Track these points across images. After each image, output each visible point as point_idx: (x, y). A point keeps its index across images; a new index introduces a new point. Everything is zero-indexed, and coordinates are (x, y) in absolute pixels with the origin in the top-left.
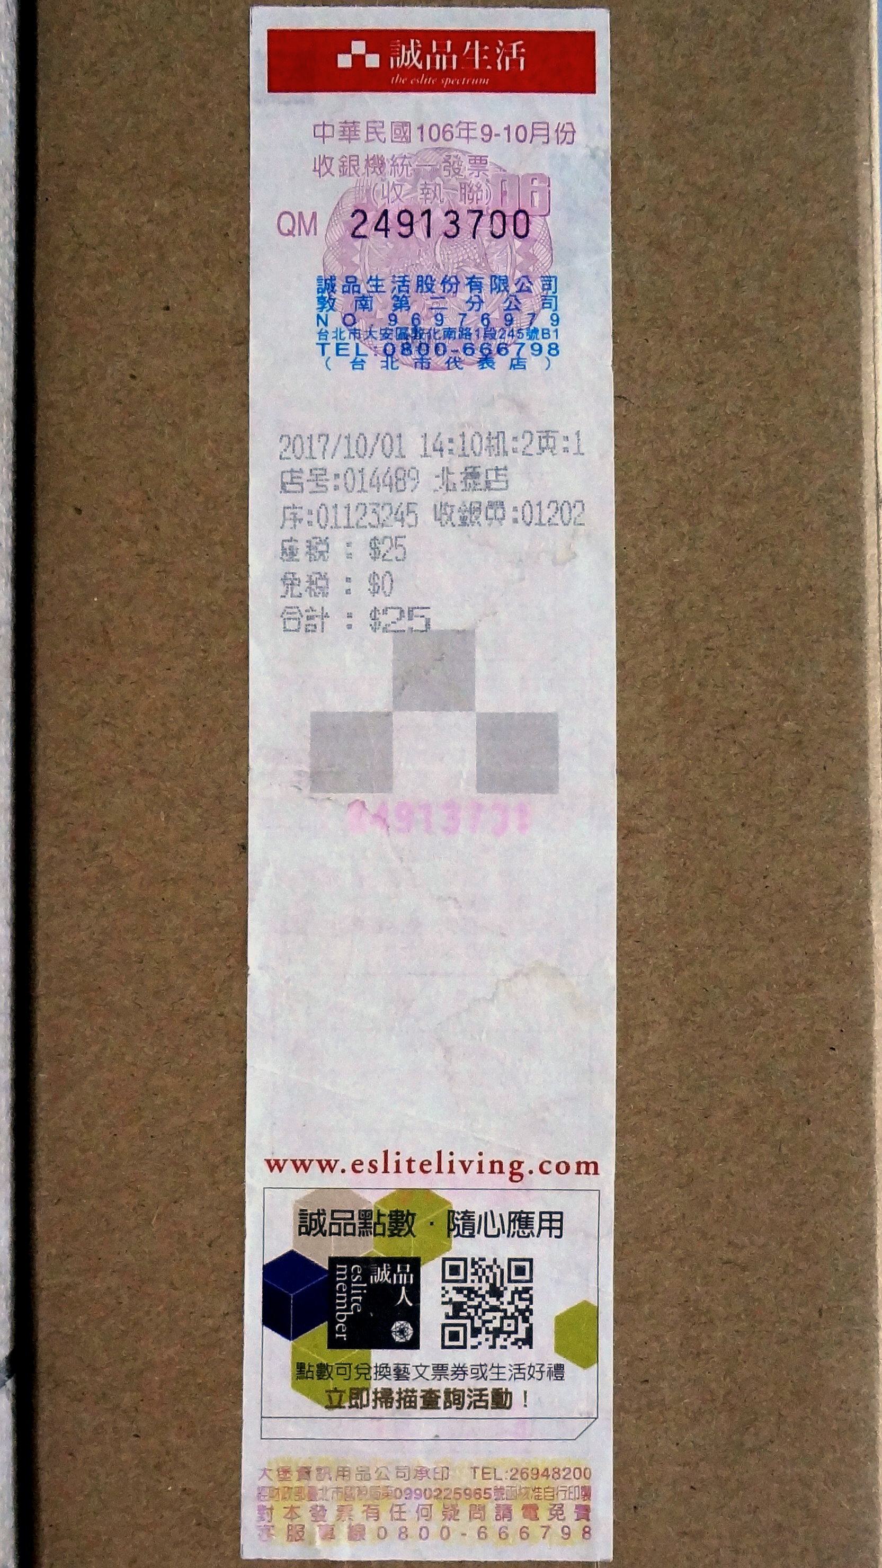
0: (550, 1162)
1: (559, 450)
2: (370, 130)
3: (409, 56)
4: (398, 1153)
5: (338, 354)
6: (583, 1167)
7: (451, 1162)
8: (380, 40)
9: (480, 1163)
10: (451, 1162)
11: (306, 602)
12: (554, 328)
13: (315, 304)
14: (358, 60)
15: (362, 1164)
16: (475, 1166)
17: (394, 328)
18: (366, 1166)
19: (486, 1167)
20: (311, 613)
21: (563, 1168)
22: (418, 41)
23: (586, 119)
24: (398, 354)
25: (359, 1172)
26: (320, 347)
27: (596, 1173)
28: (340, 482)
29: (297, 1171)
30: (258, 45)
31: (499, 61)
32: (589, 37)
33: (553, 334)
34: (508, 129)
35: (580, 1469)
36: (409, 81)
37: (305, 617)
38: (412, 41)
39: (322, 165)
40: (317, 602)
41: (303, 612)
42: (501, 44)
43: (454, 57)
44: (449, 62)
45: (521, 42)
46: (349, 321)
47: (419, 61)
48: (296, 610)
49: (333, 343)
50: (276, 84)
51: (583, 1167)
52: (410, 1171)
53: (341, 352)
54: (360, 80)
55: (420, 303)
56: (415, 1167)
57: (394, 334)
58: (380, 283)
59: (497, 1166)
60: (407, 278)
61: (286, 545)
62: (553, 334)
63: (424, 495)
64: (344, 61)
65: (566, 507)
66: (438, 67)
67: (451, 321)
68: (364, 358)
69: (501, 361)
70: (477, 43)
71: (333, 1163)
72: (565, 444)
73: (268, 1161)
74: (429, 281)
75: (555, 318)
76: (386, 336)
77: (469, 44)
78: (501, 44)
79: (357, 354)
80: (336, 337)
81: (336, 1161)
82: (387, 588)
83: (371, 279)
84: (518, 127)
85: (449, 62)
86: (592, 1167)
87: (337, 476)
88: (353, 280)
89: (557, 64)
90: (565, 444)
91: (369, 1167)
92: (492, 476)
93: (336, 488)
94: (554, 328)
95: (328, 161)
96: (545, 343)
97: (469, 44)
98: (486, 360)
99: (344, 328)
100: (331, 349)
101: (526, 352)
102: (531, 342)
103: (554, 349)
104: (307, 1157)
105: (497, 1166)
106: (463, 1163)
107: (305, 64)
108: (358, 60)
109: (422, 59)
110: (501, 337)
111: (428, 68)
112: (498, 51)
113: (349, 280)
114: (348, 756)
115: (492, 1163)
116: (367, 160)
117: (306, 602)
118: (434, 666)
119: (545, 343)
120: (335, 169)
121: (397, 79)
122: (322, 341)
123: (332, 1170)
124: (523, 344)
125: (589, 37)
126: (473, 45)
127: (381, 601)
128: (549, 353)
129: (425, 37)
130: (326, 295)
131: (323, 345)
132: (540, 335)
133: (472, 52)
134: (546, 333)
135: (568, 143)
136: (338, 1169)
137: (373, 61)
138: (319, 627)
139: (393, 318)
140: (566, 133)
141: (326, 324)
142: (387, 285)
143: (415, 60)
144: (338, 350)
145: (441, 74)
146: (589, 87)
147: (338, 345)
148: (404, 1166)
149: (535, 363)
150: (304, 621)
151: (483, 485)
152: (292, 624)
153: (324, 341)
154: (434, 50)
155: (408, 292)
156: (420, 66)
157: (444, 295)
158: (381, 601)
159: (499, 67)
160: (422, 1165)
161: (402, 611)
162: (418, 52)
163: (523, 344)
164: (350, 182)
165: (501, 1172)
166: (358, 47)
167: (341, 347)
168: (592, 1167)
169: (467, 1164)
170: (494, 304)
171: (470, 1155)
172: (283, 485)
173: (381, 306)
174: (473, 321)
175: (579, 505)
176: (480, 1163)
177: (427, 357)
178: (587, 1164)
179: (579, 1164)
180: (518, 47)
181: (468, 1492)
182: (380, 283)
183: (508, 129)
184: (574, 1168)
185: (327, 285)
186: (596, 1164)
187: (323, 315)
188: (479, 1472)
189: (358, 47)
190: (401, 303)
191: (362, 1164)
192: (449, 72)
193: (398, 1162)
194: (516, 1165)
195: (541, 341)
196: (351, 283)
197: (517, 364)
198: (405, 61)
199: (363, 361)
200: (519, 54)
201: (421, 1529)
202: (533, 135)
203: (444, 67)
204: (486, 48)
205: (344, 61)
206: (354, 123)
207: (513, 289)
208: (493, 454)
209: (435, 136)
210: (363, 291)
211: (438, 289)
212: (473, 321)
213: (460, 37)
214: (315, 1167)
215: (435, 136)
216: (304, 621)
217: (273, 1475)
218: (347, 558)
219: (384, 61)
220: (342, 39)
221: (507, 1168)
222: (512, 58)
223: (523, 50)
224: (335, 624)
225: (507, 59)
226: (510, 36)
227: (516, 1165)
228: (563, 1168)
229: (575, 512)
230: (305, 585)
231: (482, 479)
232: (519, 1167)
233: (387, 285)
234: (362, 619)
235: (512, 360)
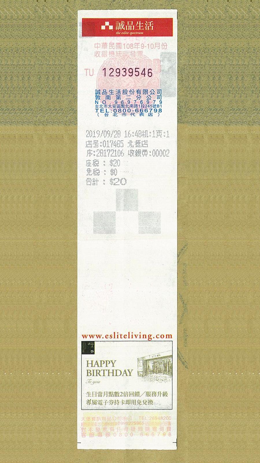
0: (159, 335)
1: (162, 136)
2: (110, 45)
3: (121, 26)
4: (132, 333)
5: (101, 112)
6: (168, 336)
7: (132, 335)
8: (113, 21)
9: (140, 335)
10: (132, 335)
11: (92, 177)
12: (161, 104)
13: (95, 98)
14: (107, 27)
15: (108, 336)
16: (139, 336)
17: (116, 105)
18: (109, 336)
19: (142, 336)
20: (94, 180)
21: (162, 336)
22: (124, 22)
23: (171, 43)
24: (117, 112)
25: (107, 338)
26: (86, 70)
27: (171, 338)
28: (102, 144)
29: (91, 338)
30: (80, 21)
31: (146, 27)
32: (170, 21)
33: (160, 106)
34: (148, 45)
35: (168, 417)
36: (121, 33)
37: (92, 181)
38: (122, 22)
39: (97, 54)
40: (96, 177)
41: (92, 180)
42: (147, 22)
43: (134, 26)
44: (132, 27)
45: (152, 22)
46: (104, 102)
47: (124, 27)
48: (90, 179)
49: (100, 109)
50: (84, 35)
51: (168, 336)
52: (121, 338)
53: (102, 111)
54: (108, 33)
55: (124, 98)
56: (122, 336)
57: (116, 106)
58: (112, 92)
59: (144, 336)
60: (120, 90)
61: (88, 162)
62: (160, 106)
63: (126, 149)
64: (103, 28)
65: (164, 152)
66: (129, 29)
67: (132, 102)
68: (108, 113)
69: (146, 114)
70: (140, 22)
71: (100, 336)
72: (164, 134)
73: (83, 335)
74: (126, 91)
75: (161, 102)
76: (114, 107)
77: (138, 22)
78: (147, 22)
79: (106, 112)
80: (101, 107)
81: (101, 335)
82: (115, 173)
83: (110, 91)
84: (151, 44)
85: (132, 27)
86: (170, 336)
87: (101, 143)
88: (105, 91)
89: (162, 28)
90: (164, 134)
91: (112, 336)
92: (144, 143)
93: (101, 146)
94: (161, 104)
95: (99, 53)
96: (158, 109)
97: (138, 22)
98: (141, 114)
99: (103, 104)
100: (99, 111)
101: (153, 111)
102: (154, 108)
103: (160, 110)
104: (93, 334)
105: (144, 336)
106: (135, 335)
107: (92, 28)
108: (107, 27)
109: (125, 27)
110: (146, 107)
111: (126, 29)
112: (146, 24)
113: (104, 91)
114: (105, 225)
115: (143, 335)
116: (109, 52)
117: (92, 177)
118: (128, 199)
119: (158, 109)
120: (100, 55)
121: (118, 33)
122: (97, 108)
123: (100, 338)
124: (152, 109)
125: (170, 21)
126: (139, 23)
127: (114, 177)
128: (159, 111)
129: (126, 20)
130: (98, 95)
131: (97, 109)
132: (156, 107)
133: (138, 25)
134: (158, 106)
135: (165, 49)
136: (101, 337)
137: (111, 28)
138: (96, 184)
139: (116, 102)
140: (165, 46)
141: (98, 103)
142: (115, 93)
143: (123, 28)
144: (101, 111)
145: (129, 31)
146: (170, 34)
147: (101, 109)
148: (119, 336)
149: (155, 115)
150: (92, 182)
151: (141, 146)
152: (89, 183)
153: (97, 108)
154: (128, 24)
155: (120, 94)
156: (124, 29)
157: (130, 95)
158: (114, 177)
159: (146, 29)
160: (124, 336)
161: (119, 180)
162: (124, 25)
163: (152, 109)
164: (105, 59)
165: (146, 338)
166: (107, 23)
167: (102, 110)
168: (170, 336)
169: (136, 336)
170: (144, 98)
171: (137, 333)
172: (87, 145)
173: (113, 98)
174: (138, 102)
175: (168, 151)
176: (140, 335)
177: (126, 113)
178: (169, 335)
179: (167, 335)
180: (151, 23)
181: (138, 423)
182: (112, 92)
183: (148, 45)
184: (165, 336)
185: (98, 92)
186: (171, 335)
187: (97, 101)
188: (141, 418)
189: (107, 23)
190: (118, 98)
191: (108, 336)
192: (132, 31)
193: (118, 335)
194: (150, 336)
195: (157, 108)
196: (105, 92)
197: (150, 115)
198: (120, 28)
199: (108, 114)
200: (151, 25)
201: (125, 433)
202: (155, 47)
203: (131, 29)
204: (142, 23)
205: (103, 28)
206: (106, 43)
207: (149, 94)
208: (144, 136)
209: (128, 47)
210: (108, 94)
211: (128, 93)
212: (138, 102)
213: (135, 20)
214: (88, 337)
215: (128, 47)
216: (92, 182)
217: (85, 419)
218: (104, 167)
219: (114, 27)
220: (102, 21)
221: (147, 337)
222: (150, 26)
223: (153, 24)
224: (100, 183)
225: (148, 27)
226: (149, 20)
227: (150, 336)
228: (162, 336)
229: (167, 153)
230: (92, 172)
231: (141, 144)
232: (151, 336)
233: (115, 93)
234: (108, 181)
235: (149, 113)
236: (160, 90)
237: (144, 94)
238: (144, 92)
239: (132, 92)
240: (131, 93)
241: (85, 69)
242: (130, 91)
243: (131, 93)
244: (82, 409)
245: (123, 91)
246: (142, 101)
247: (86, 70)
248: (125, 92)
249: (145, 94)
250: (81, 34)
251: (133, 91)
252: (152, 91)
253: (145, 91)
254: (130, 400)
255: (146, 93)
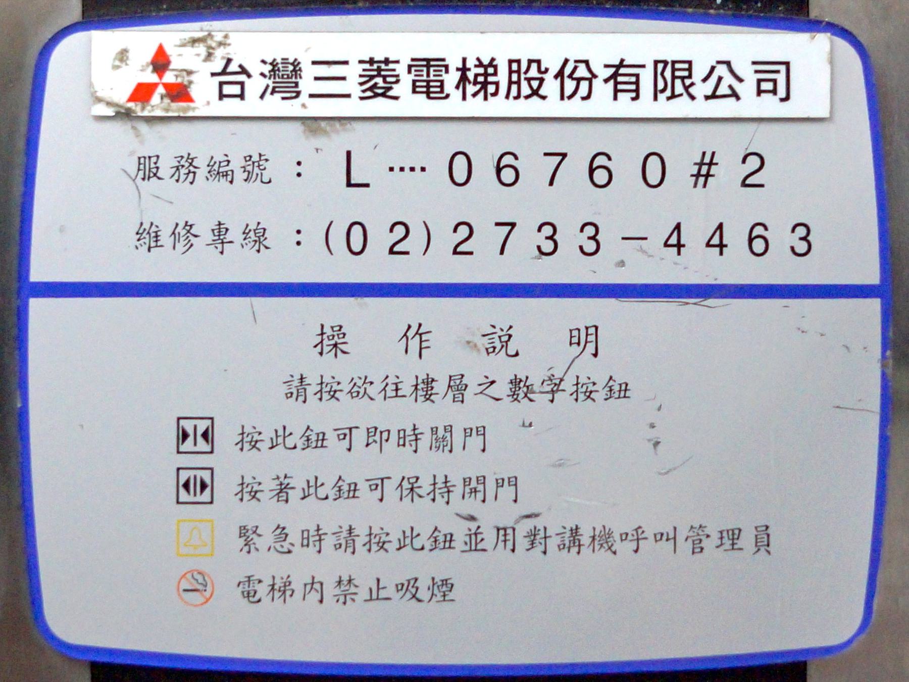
74: (533, 72)
236: (783, 68)
237: (662, 97)
238: (661, 86)
239: (579, 80)
240: (568, 91)
241: (615, 98)
242: (560, 74)
243: (570, 86)
244: (209, 500)
245: (466, 481)
246: (758, 230)
247: (619, 94)
248: (529, 80)
249: (673, 96)
250: (808, 667)
251: (582, 72)
252: (722, 70)
253: (668, 74)
254: (507, 97)
255: (679, 89)
